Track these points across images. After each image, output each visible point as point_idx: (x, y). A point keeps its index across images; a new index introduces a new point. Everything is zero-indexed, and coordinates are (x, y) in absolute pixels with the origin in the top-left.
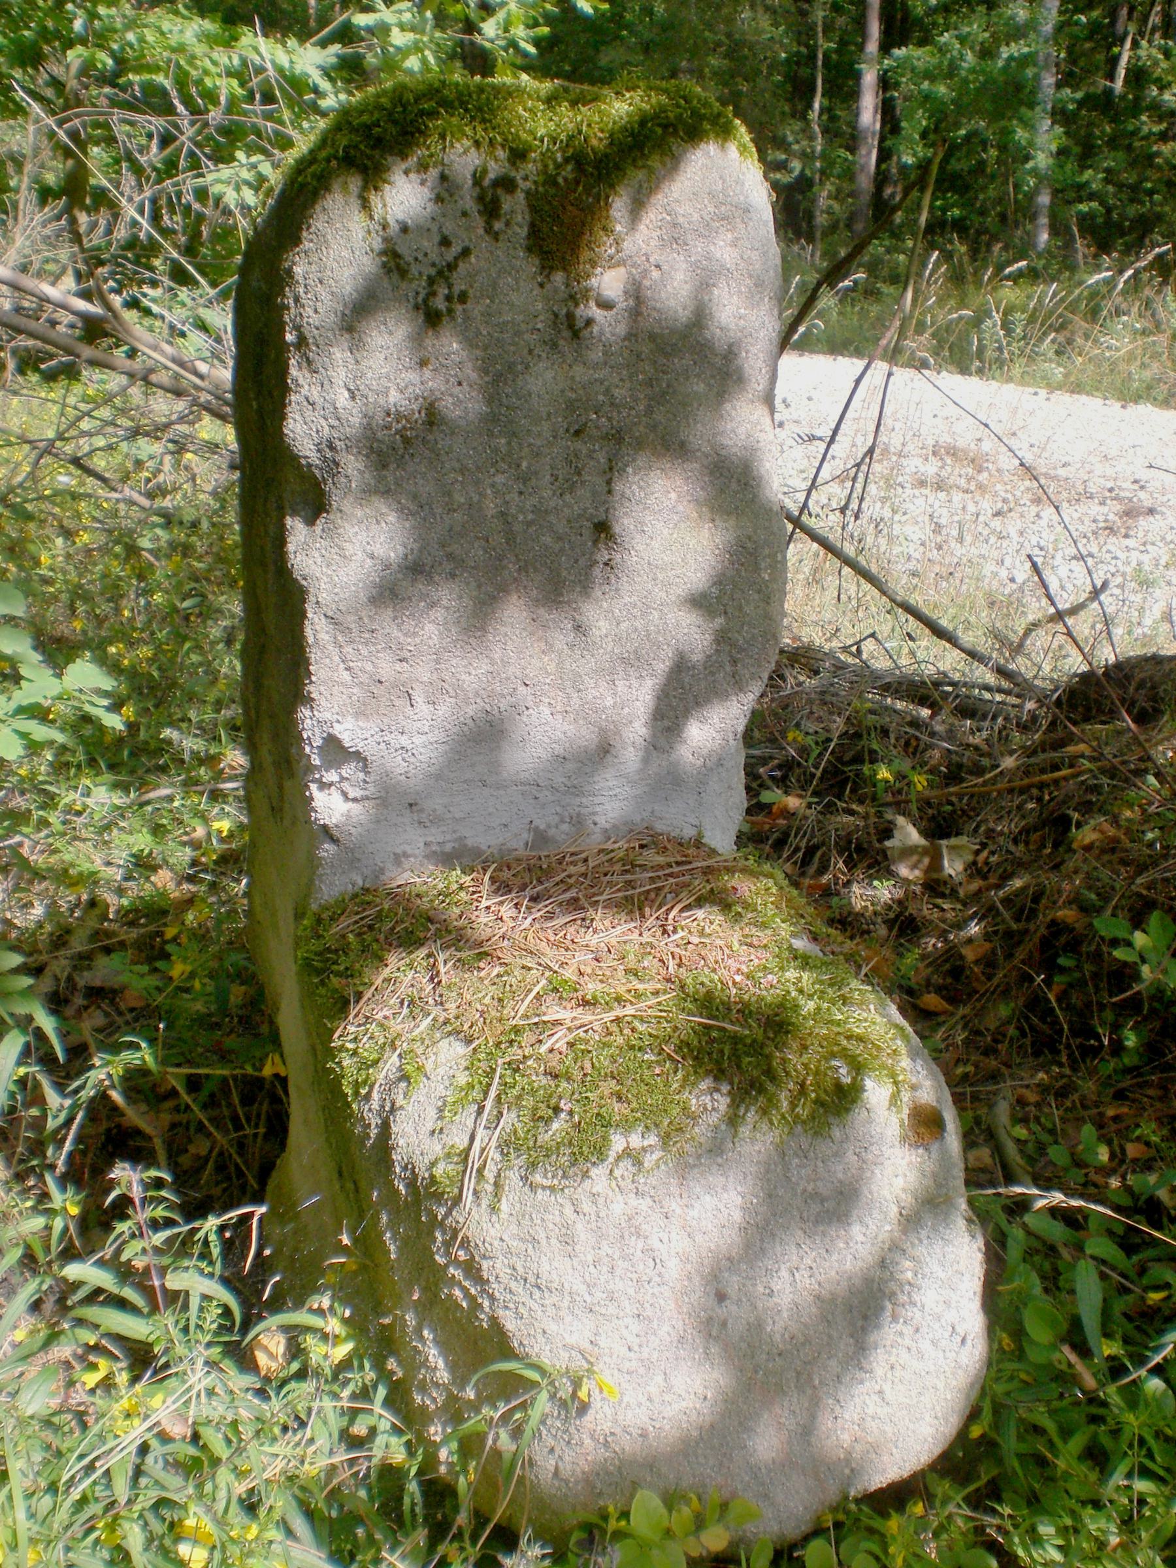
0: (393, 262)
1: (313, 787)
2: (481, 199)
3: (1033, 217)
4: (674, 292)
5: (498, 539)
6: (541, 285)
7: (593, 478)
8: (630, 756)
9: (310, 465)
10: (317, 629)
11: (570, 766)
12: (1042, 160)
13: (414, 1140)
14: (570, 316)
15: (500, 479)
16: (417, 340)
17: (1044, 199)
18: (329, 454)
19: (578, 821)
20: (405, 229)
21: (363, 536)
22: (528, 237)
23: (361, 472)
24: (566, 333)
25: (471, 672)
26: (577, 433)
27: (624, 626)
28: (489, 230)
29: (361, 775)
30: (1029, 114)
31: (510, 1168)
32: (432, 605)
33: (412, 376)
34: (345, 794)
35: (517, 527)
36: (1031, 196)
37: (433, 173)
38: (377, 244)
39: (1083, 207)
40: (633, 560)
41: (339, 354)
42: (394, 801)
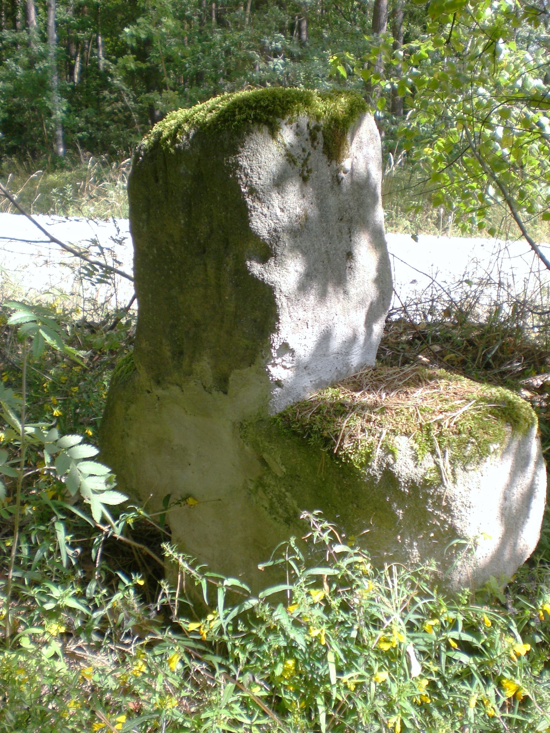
0: (290, 158)
1: (270, 367)
2: (310, 134)
3: (56, 141)
4: (361, 168)
5: (326, 262)
6: (329, 166)
7: (346, 236)
8: (361, 339)
9: (264, 239)
10: (281, 301)
11: (347, 344)
12: (59, 114)
13: (407, 471)
14: (337, 176)
15: (324, 239)
16: (301, 187)
17: (60, 133)
18: (274, 234)
19: (347, 365)
20: (292, 146)
21: (293, 264)
22: (323, 148)
23: (289, 240)
24: (336, 183)
25: (323, 313)
26: (341, 220)
27: (359, 289)
28: (312, 146)
29: (291, 358)
30: (51, 93)
31: (457, 467)
32: (312, 288)
33: (301, 201)
34: (285, 367)
35: (331, 256)
36: (53, 132)
37: (294, 124)
38: (283, 152)
39: (79, 135)
40: (358, 265)
41: (274, 195)
42: (302, 368)
